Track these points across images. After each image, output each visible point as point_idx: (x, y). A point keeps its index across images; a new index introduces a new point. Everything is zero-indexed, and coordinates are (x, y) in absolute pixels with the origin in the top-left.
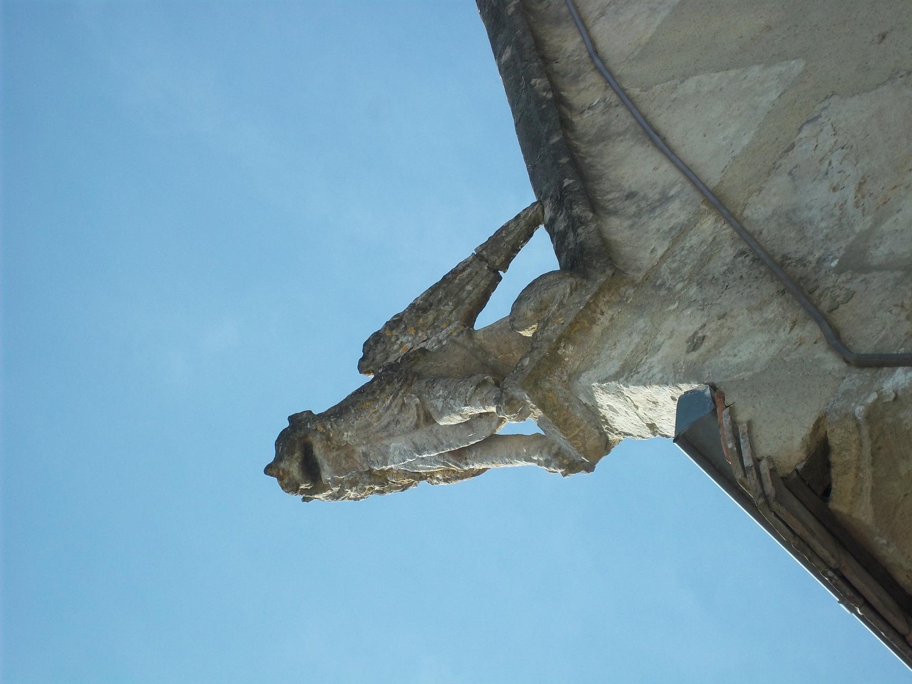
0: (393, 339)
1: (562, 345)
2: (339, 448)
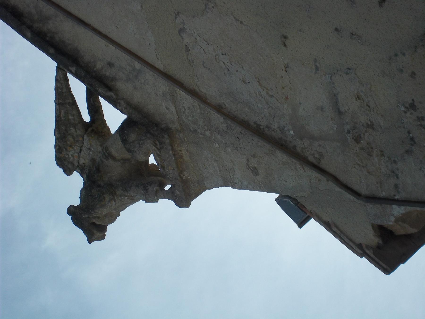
0: (67, 156)
1: (182, 176)
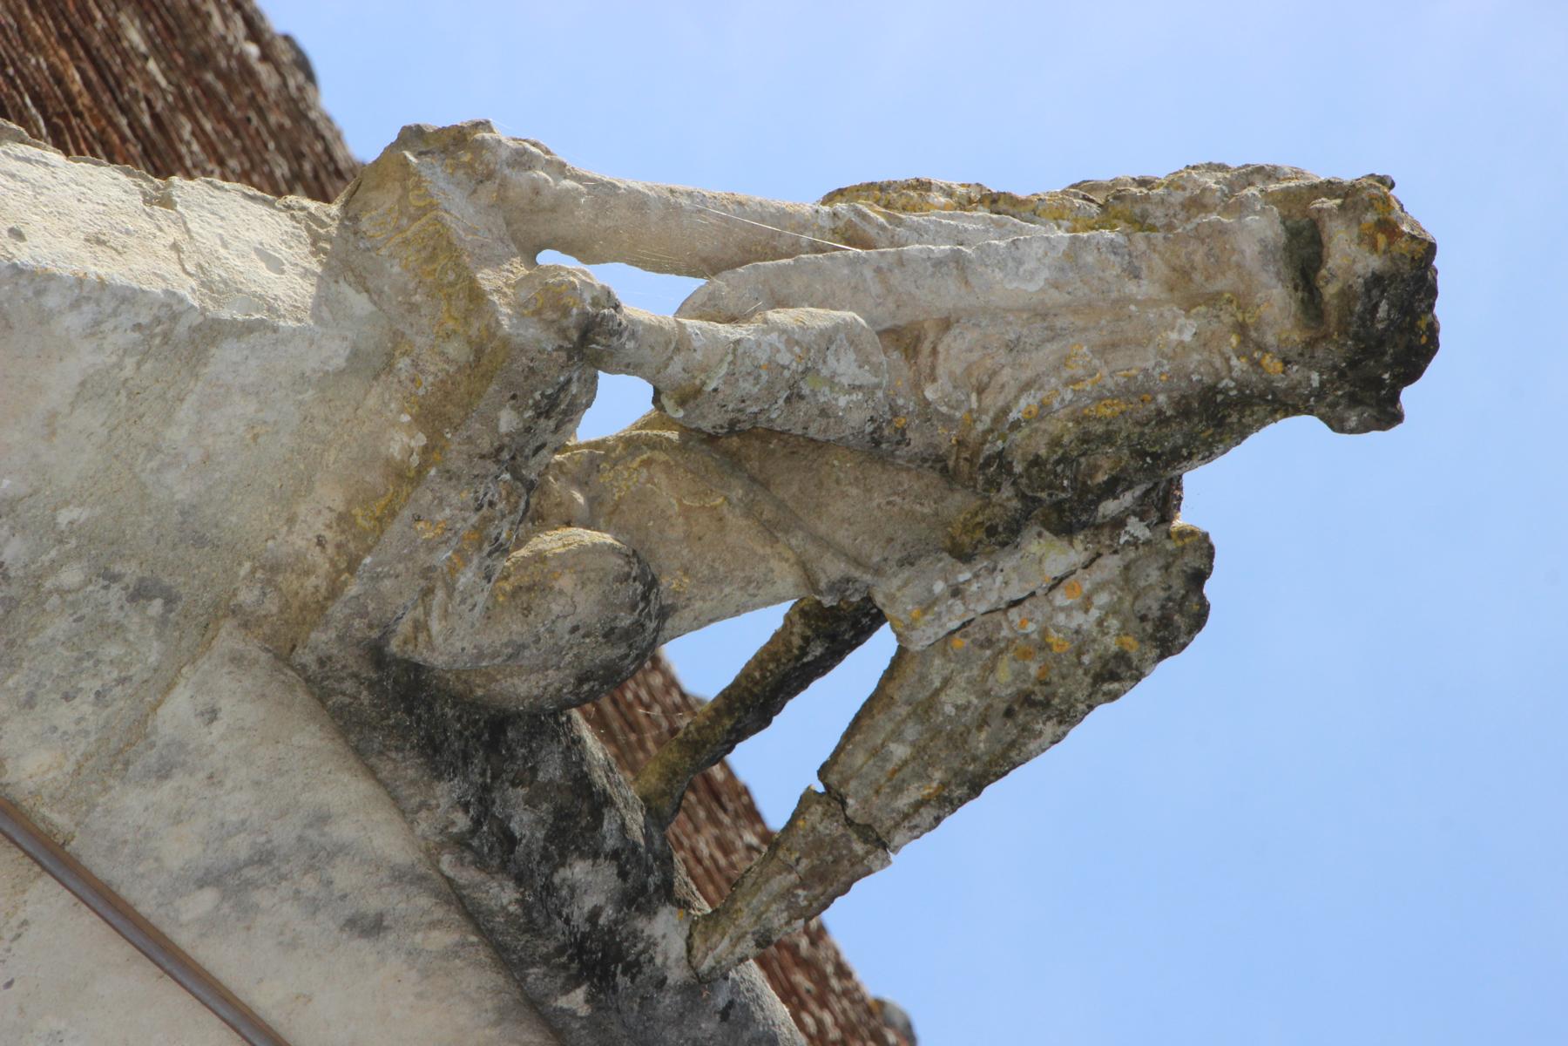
0: (1114, 623)
1: (415, 460)
2: (1213, 299)
